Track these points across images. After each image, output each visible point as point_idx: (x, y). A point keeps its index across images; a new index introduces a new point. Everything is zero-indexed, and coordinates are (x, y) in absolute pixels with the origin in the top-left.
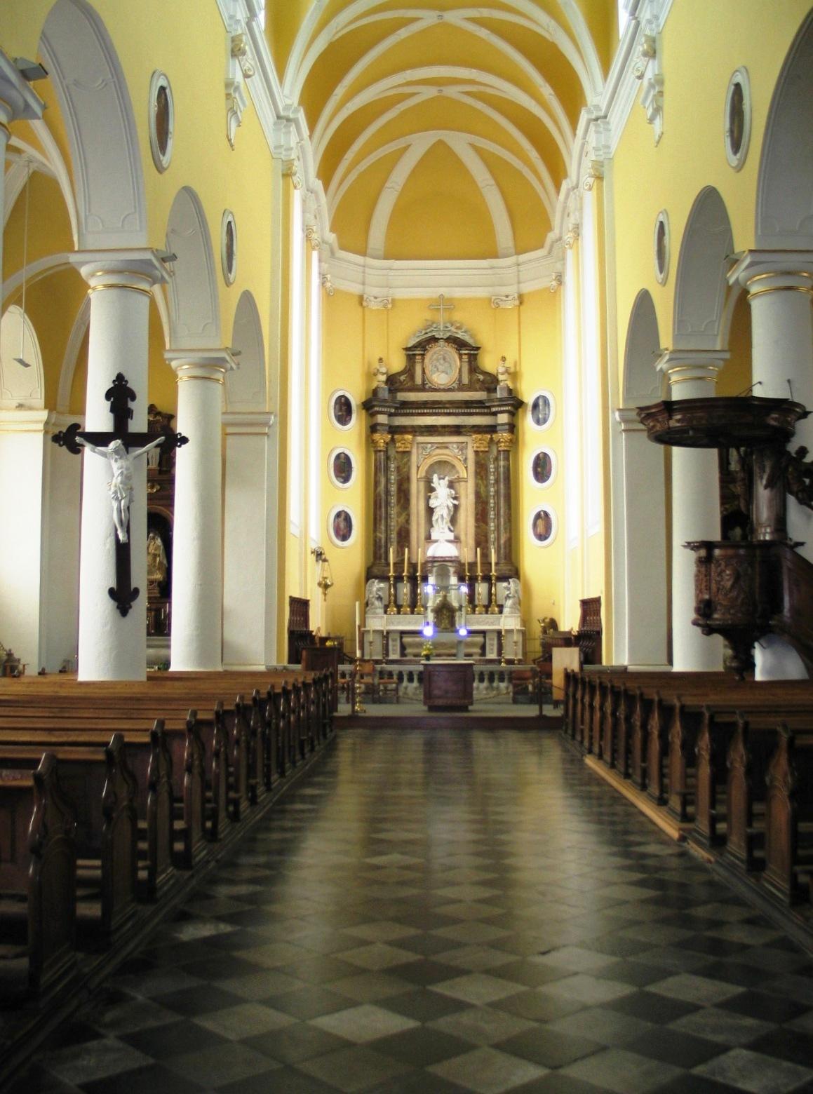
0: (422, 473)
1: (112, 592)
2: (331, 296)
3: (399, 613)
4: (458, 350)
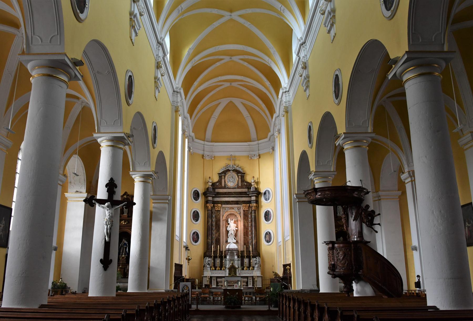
0: (224, 218)
1: (101, 261)
3: (215, 269)
4: (237, 174)
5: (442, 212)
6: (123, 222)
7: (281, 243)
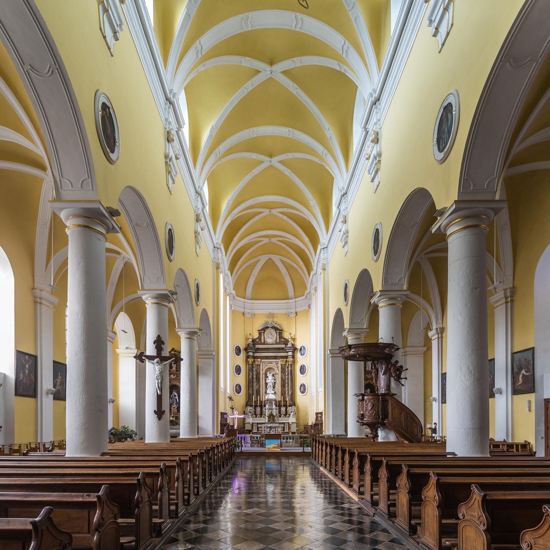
0: (264, 371)
2: (233, 312)
3: (256, 417)
5: (470, 368)
6: (172, 376)
7: (315, 394)
